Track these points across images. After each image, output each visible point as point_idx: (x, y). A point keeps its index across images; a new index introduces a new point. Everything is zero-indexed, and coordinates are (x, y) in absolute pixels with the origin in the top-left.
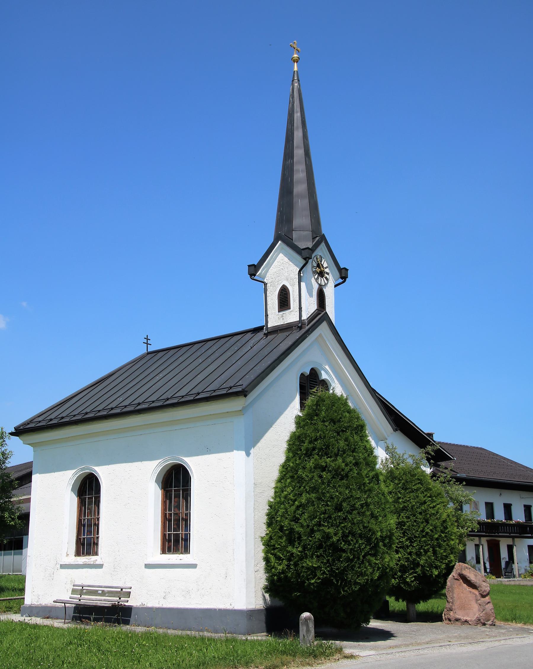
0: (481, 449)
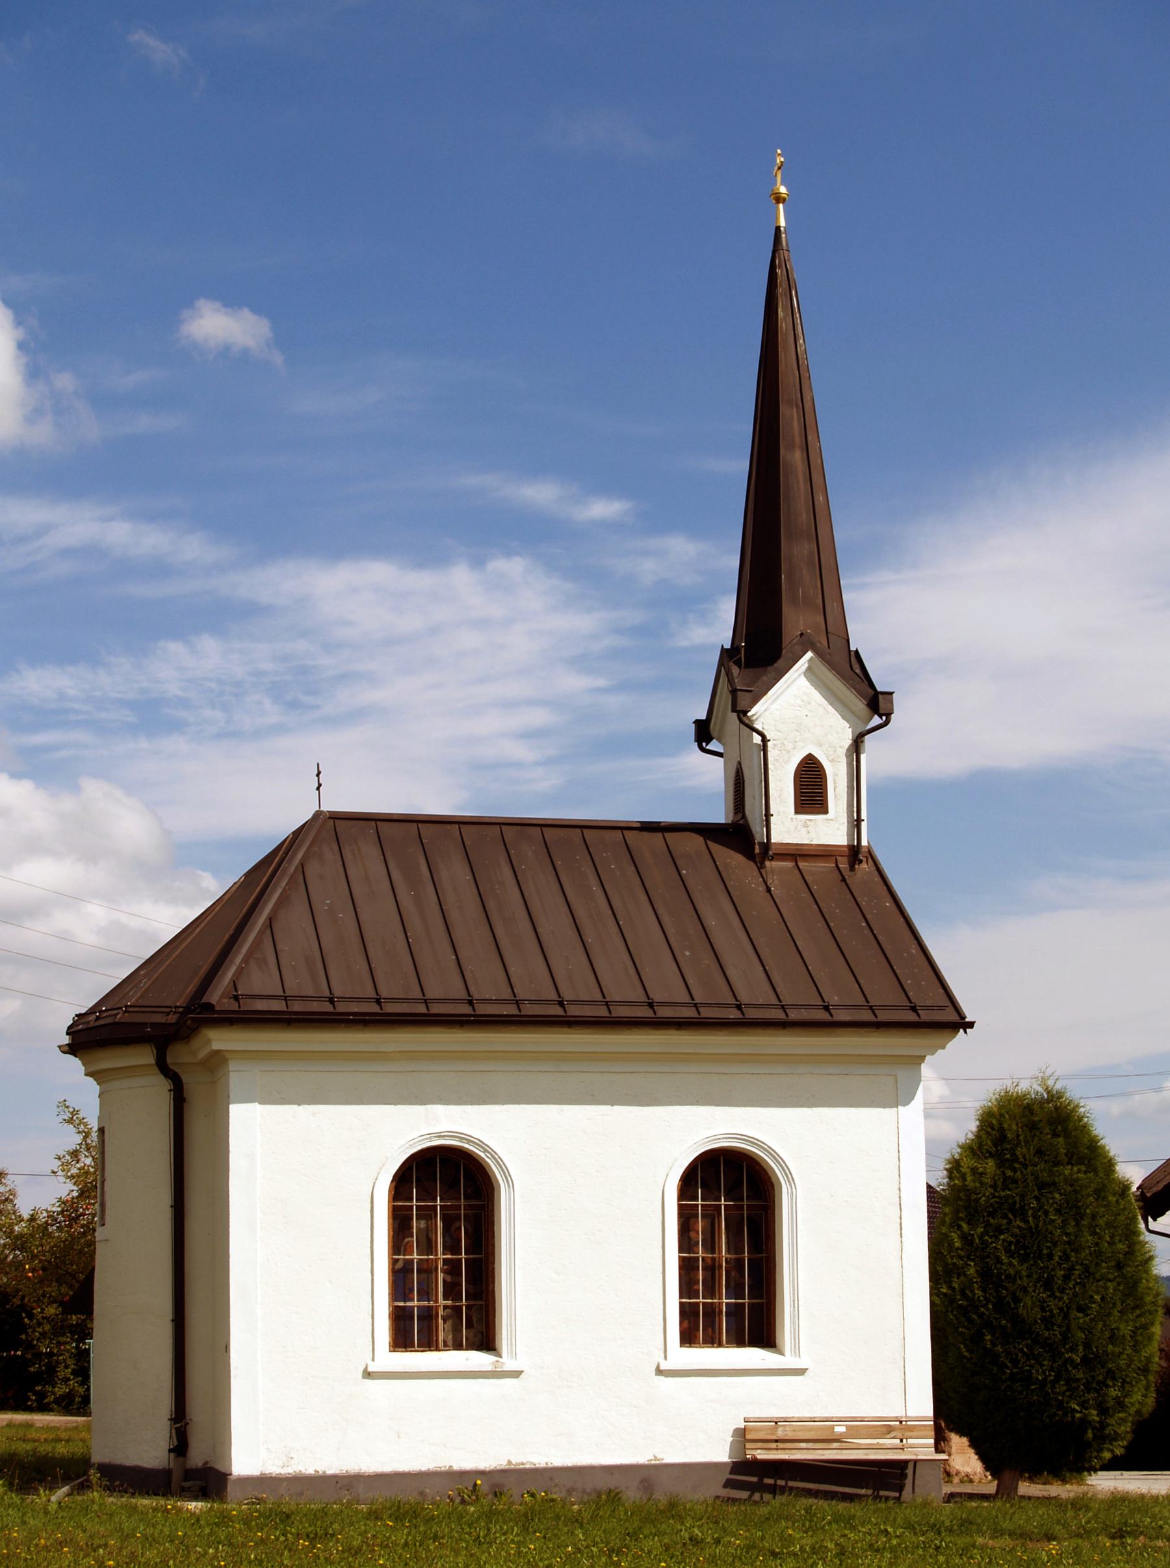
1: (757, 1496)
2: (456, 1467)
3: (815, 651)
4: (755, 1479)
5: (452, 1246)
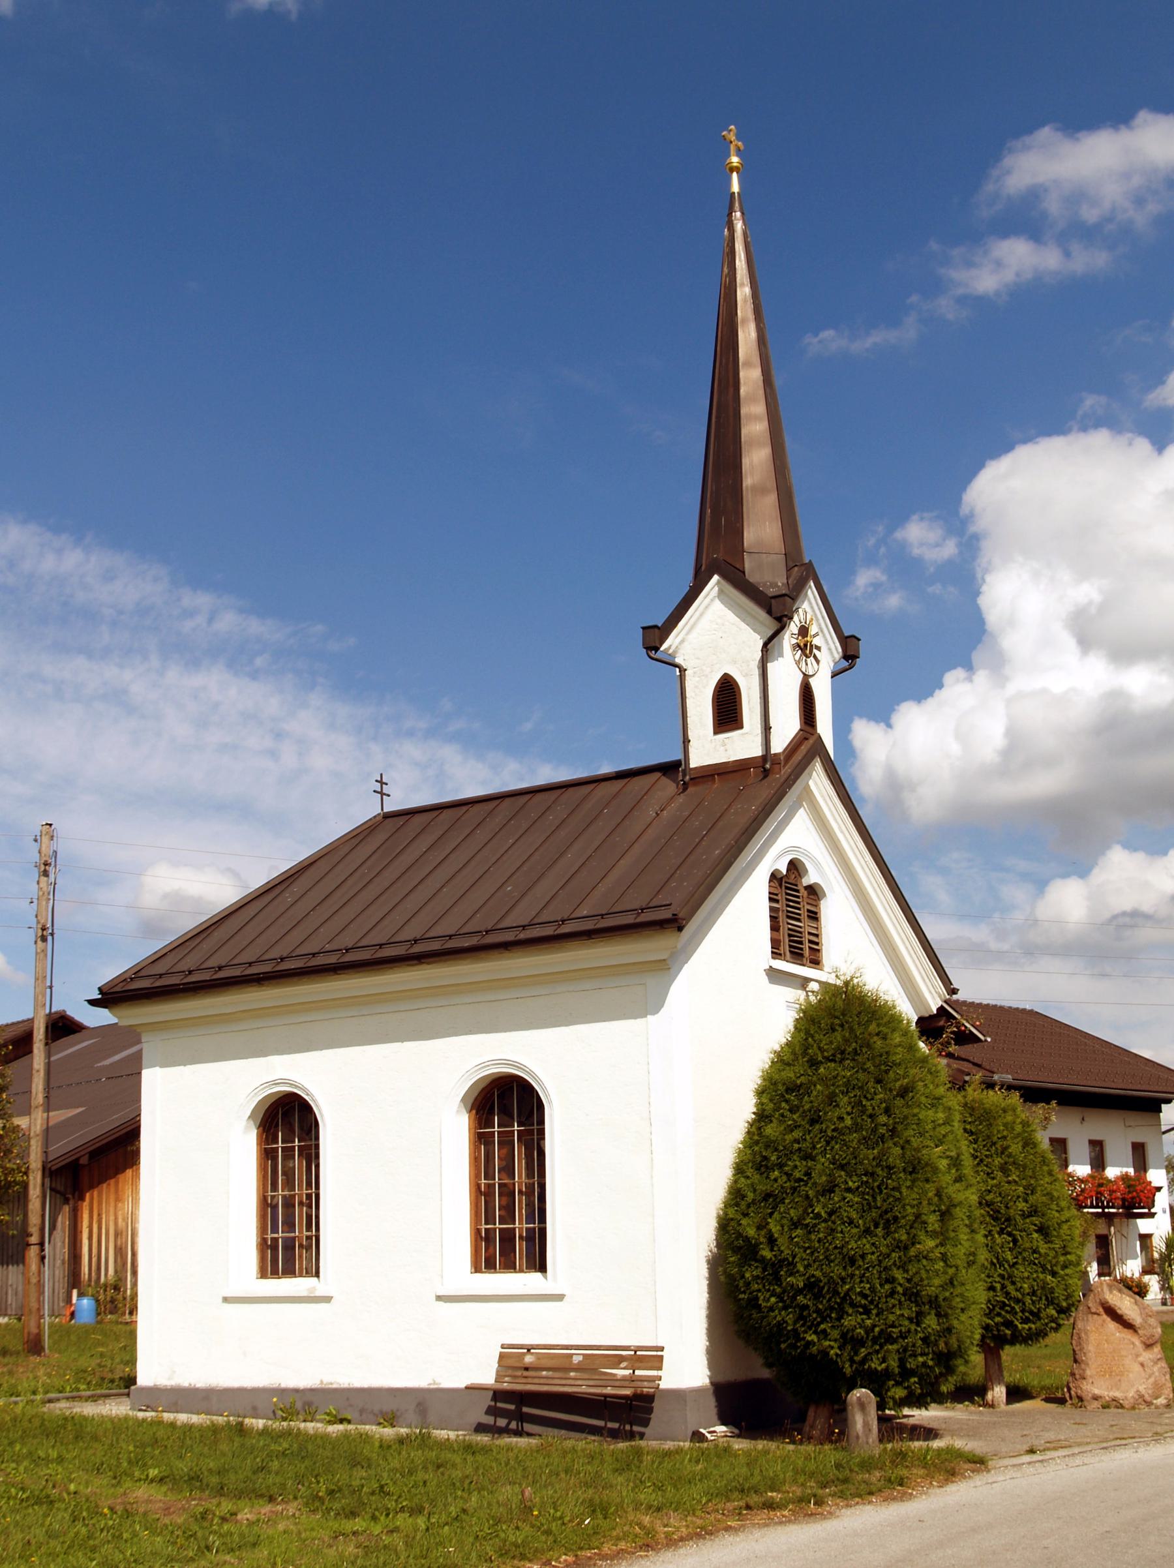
0: (1032, 1013)
2: (283, 1386)
4: (512, 1407)
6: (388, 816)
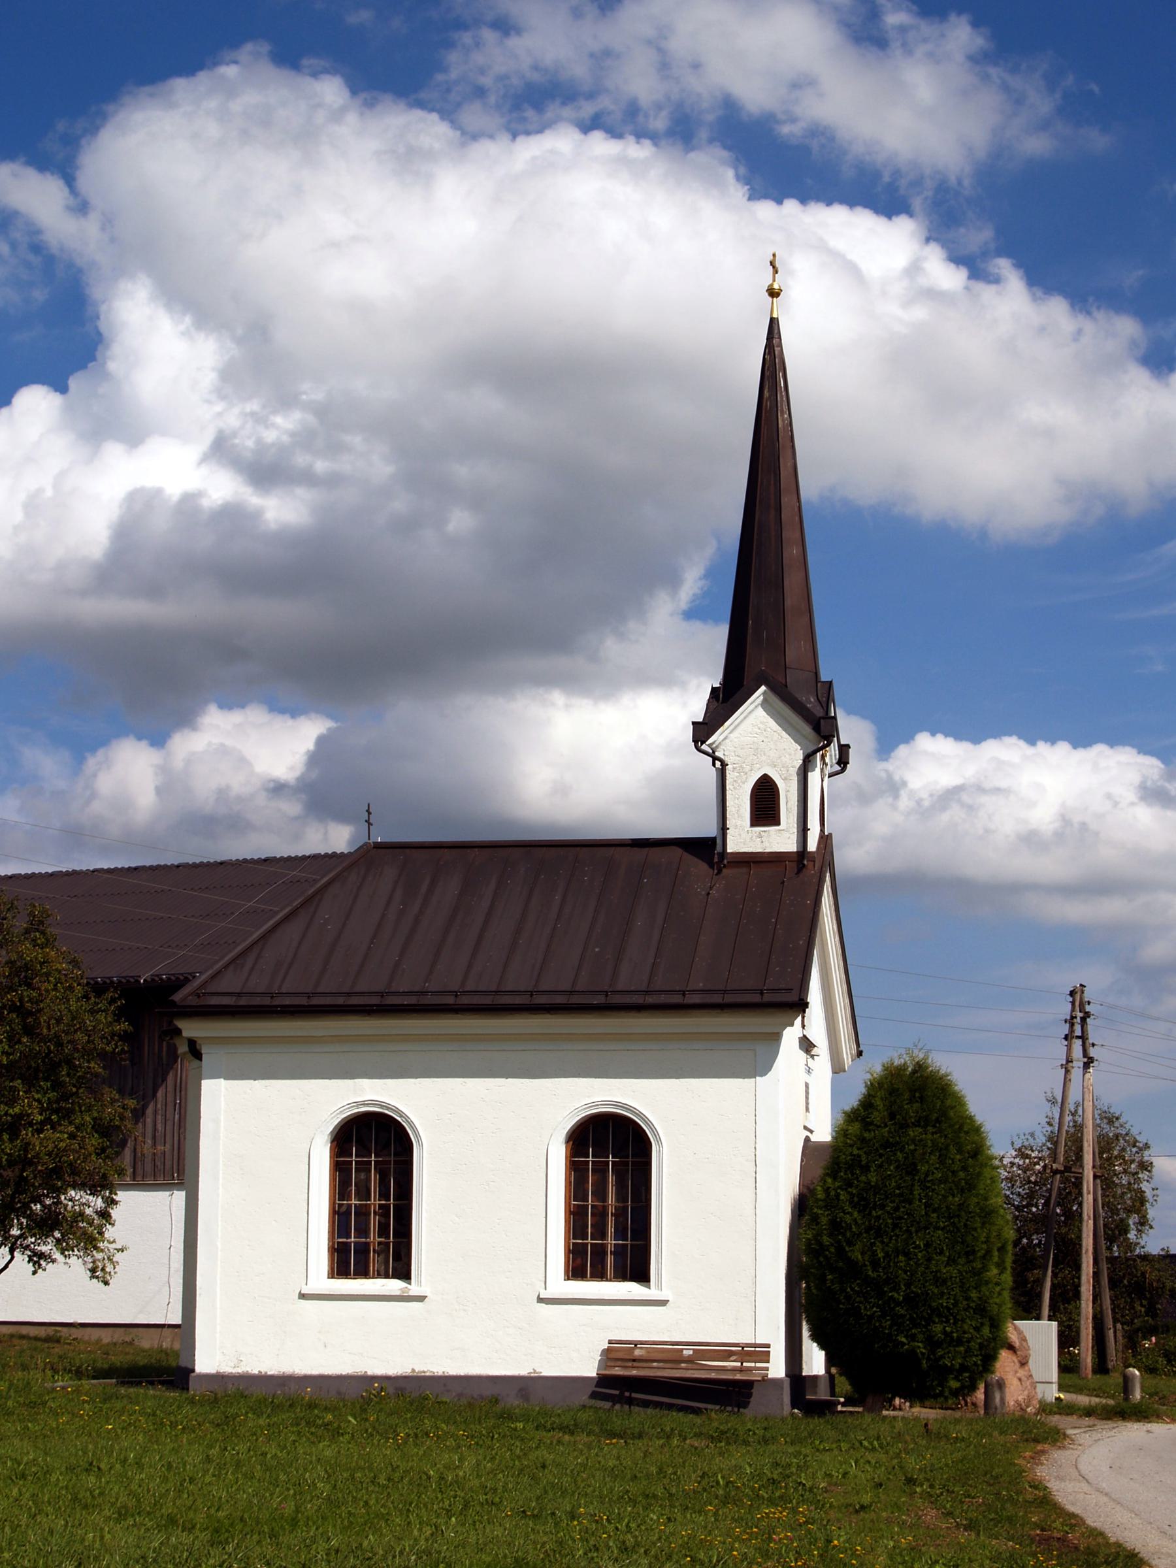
1: (617, 1407)
2: (370, 1373)
3: (766, 685)
4: (617, 1392)
5: (384, 1195)
6: (377, 846)
